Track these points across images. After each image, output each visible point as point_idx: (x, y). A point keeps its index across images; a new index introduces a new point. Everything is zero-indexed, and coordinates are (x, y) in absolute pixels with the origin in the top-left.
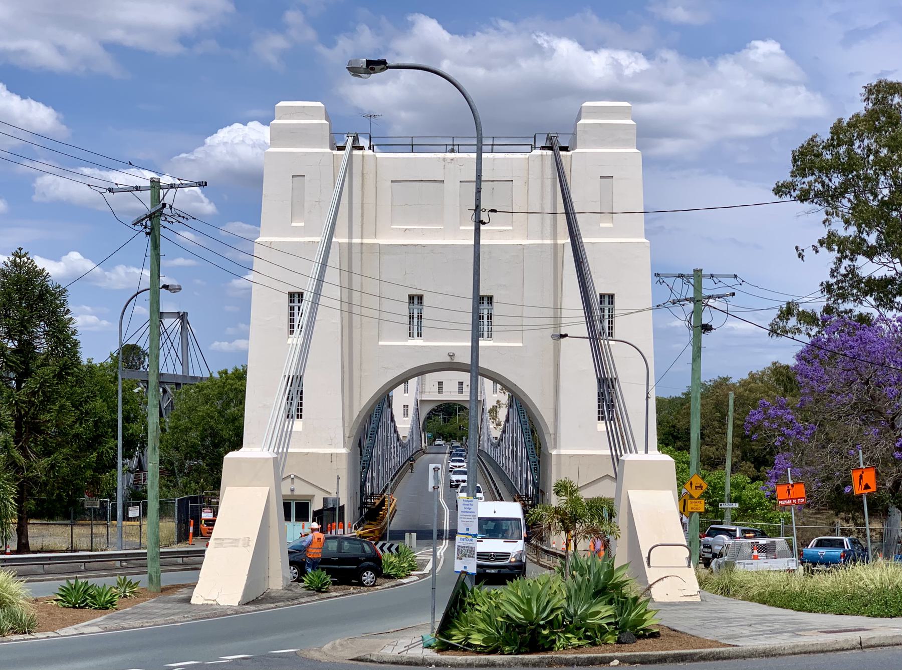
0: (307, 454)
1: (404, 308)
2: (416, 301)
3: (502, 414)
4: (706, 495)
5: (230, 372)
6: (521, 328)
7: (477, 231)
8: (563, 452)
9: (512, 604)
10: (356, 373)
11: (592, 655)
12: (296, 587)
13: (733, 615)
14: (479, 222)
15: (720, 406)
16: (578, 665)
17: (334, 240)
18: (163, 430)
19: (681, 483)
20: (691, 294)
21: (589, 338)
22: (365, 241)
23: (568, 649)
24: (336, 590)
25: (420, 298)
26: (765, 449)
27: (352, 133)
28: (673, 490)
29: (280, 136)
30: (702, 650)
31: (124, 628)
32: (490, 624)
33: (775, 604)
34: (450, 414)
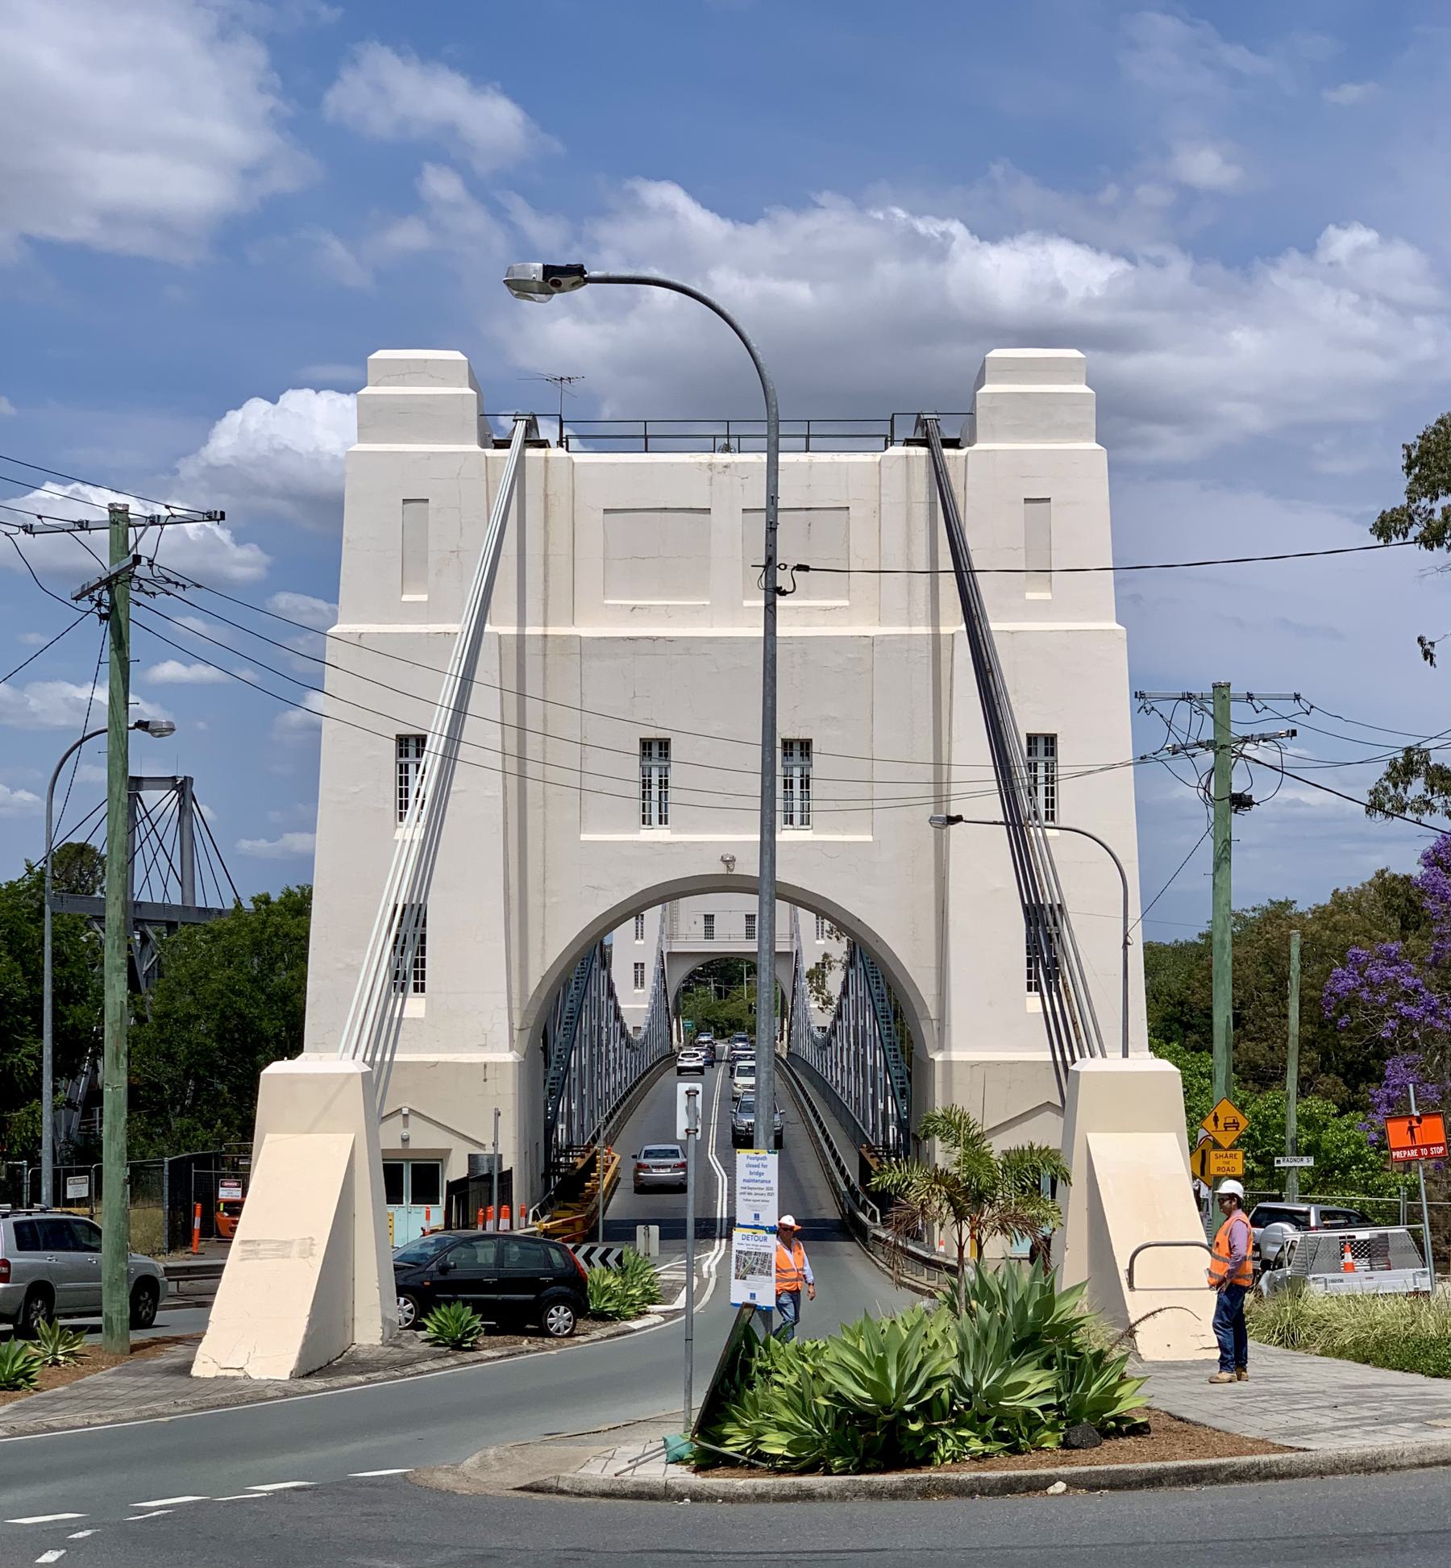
0: (435, 1064)
1: (632, 767)
2: (655, 751)
3: (834, 982)
4: (1247, 1142)
5: (275, 898)
6: (868, 804)
7: (770, 609)
8: (957, 1056)
9: (845, 1369)
10: (533, 900)
11: (1011, 1473)
12: (410, 1340)
13: (1302, 1387)
14: (774, 592)
15: (1274, 959)
16: (982, 1494)
17: (488, 628)
18: (141, 1020)
19: (1194, 1115)
20: (1208, 735)
21: (1007, 824)
22: (551, 631)
23: (962, 1457)
24: (492, 1346)
25: (664, 744)
26: (1366, 1047)
27: (521, 415)
28: (1178, 1133)
29: (376, 420)
30: (1234, 1459)
31: (54, 1429)
32: (804, 1412)
33: (1386, 1364)
34: (729, 982)
